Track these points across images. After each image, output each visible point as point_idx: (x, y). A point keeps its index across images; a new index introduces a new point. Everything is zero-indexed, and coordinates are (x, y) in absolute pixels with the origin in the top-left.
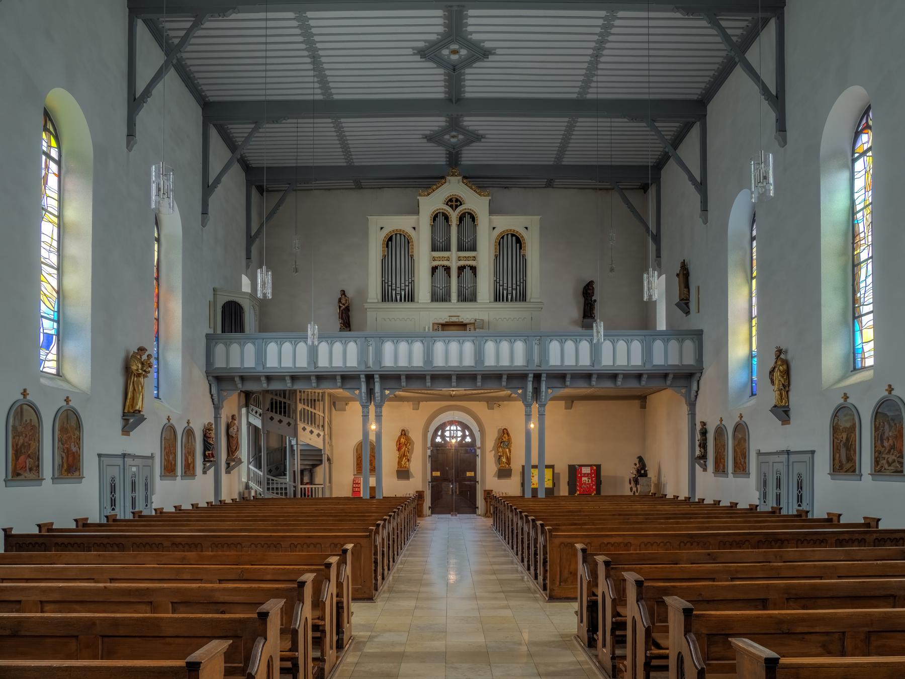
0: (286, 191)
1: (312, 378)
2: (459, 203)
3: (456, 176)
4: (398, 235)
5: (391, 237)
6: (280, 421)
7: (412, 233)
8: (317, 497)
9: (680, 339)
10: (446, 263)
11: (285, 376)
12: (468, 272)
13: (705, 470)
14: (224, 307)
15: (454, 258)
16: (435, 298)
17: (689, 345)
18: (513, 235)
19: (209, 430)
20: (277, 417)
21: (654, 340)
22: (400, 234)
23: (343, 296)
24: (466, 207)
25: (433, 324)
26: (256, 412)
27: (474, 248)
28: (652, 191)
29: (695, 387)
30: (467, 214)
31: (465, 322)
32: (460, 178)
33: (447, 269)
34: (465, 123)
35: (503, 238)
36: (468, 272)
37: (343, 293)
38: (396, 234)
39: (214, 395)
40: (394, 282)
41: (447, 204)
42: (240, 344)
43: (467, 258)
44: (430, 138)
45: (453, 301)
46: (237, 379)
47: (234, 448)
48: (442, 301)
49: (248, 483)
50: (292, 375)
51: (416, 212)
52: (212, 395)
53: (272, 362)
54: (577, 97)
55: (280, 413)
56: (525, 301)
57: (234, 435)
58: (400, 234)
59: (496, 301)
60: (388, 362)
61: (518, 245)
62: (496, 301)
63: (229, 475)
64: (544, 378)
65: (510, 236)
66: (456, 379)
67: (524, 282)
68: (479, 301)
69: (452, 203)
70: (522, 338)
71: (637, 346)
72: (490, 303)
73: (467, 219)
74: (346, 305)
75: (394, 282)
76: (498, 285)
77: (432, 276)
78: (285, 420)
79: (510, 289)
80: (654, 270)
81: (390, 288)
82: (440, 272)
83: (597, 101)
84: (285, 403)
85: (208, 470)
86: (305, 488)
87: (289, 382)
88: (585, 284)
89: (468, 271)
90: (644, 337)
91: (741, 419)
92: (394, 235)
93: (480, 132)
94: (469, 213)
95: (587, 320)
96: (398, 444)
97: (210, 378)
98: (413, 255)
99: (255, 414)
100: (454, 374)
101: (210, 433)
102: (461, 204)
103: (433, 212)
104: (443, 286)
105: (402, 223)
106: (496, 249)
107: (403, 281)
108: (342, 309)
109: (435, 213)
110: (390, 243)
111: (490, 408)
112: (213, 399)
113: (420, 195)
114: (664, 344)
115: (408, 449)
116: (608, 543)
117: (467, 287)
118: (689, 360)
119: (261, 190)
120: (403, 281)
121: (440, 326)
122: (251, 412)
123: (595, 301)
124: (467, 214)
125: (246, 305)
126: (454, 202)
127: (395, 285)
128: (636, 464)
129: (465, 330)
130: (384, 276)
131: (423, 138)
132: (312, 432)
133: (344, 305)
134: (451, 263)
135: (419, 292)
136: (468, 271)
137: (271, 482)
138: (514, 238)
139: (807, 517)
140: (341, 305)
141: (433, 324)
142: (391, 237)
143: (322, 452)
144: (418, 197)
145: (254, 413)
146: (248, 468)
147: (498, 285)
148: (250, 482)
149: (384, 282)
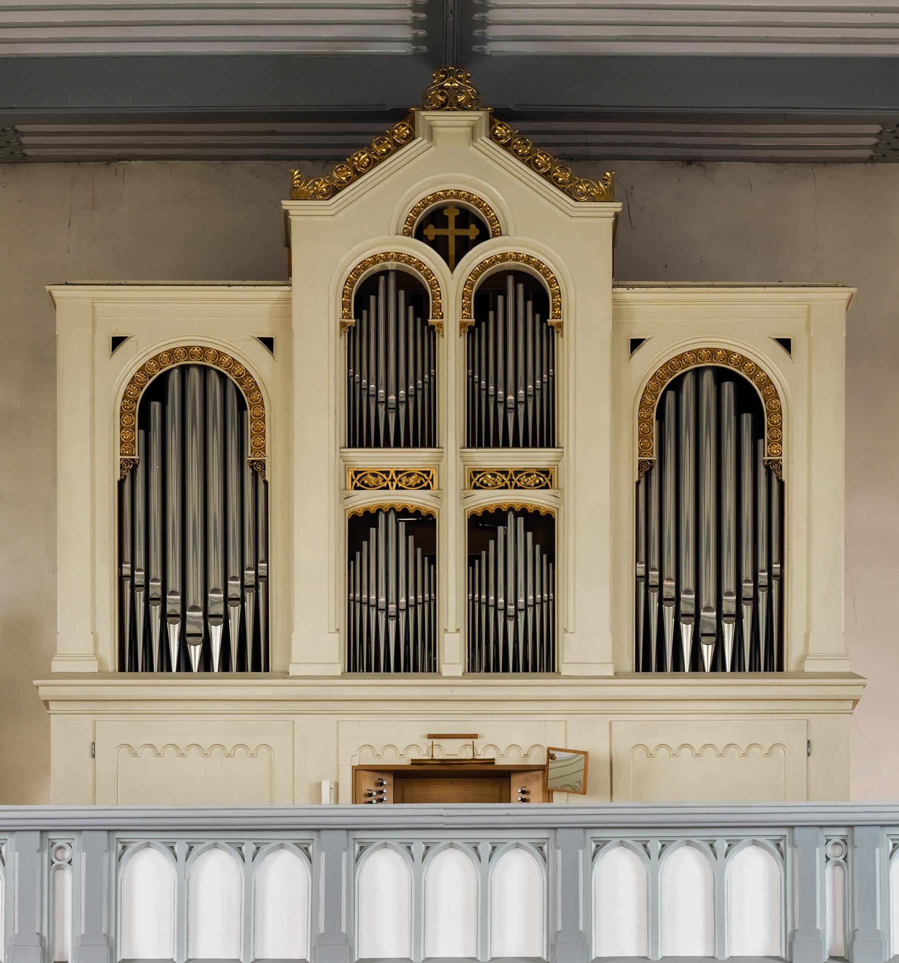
3: (461, 107)
5: (165, 377)
35: (676, 386)
61: (747, 418)
65: (708, 378)
98: (263, 463)
110: (156, 406)
138: (728, 388)
142: (164, 378)
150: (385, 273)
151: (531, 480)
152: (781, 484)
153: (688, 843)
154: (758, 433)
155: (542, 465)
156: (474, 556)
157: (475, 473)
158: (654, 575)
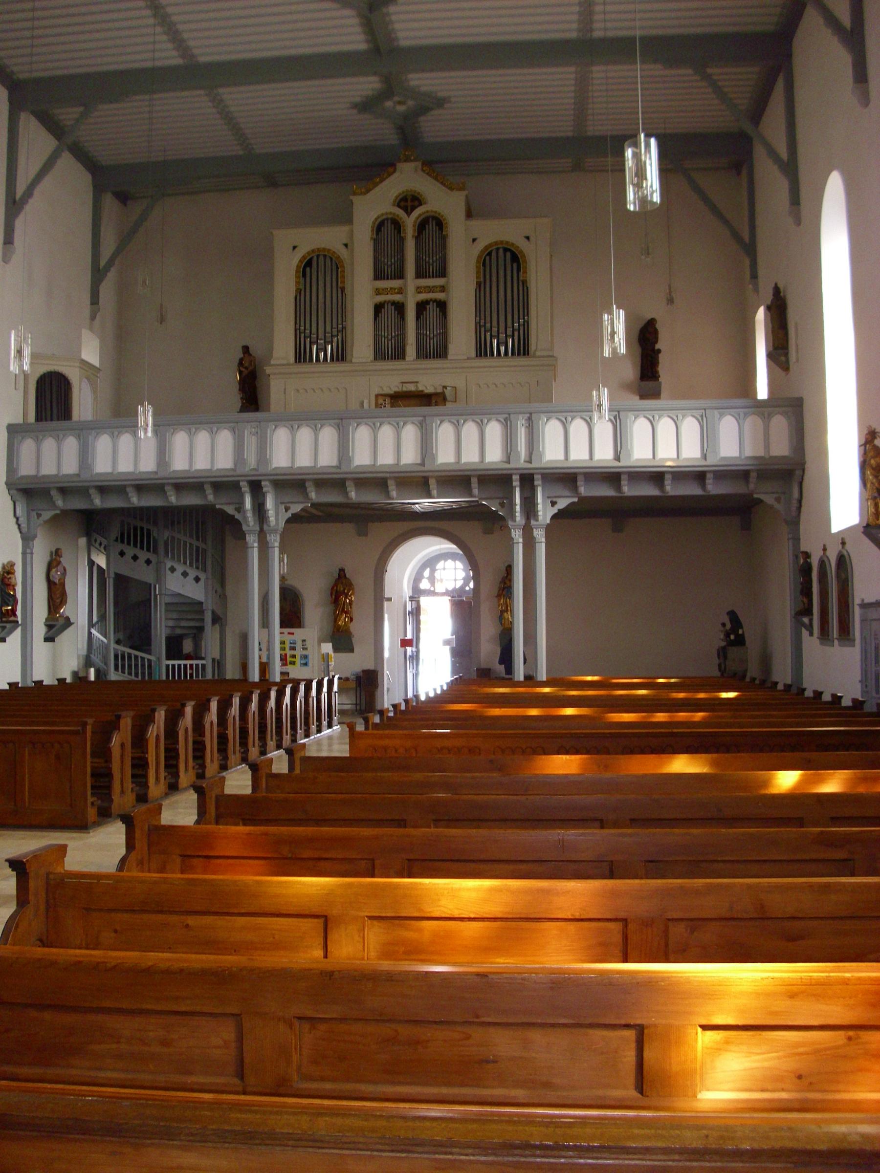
1: (166, 488)
2: (416, 203)
3: (411, 161)
4: (321, 259)
7: (343, 253)
9: (766, 414)
10: (397, 298)
11: (125, 486)
12: (432, 311)
13: (811, 634)
16: (380, 354)
17: (780, 424)
18: (506, 250)
19: (9, 573)
20: (130, 551)
21: (722, 416)
22: (325, 256)
23: (246, 355)
24: (429, 209)
25: (377, 396)
26: (100, 544)
27: (442, 272)
28: (744, 172)
29: (796, 495)
30: (431, 219)
31: (426, 391)
32: (419, 164)
33: (400, 308)
34: (412, 83)
35: (490, 254)
36: (432, 311)
38: (318, 256)
39: (20, 519)
40: (314, 330)
41: (399, 206)
42: (112, 436)
43: (431, 289)
44: (366, 106)
45: (407, 358)
46: (54, 493)
47: (58, 601)
48: (395, 359)
49: (90, 657)
50: (215, 482)
51: (345, 217)
52: (17, 519)
53: (102, 465)
55: (135, 545)
56: (528, 354)
57: (57, 581)
58: (325, 256)
59: (481, 355)
61: (515, 265)
62: (481, 355)
64: (538, 482)
66: (629, 480)
67: (526, 324)
68: (450, 357)
70: (332, 422)
71: (691, 427)
72: (468, 358)
73: (432, 226)
74: (250, 368)
75: (314, 330)
76: (483, 329)
77: (375, 319)
78: (143, 555)
79: (502, 336)
80: (618, 308)
82: (389, 313)
83: (603, 40)
84: (142, 529)
85: (8, 636)
86: (197, 665)
87: (209, 491)
88: (642, 324)
89: (432, 310)
90: (703, 411)
91: (843, 547)
92: (315, 257)
93: (440, 94)
94: (434, 218)
95: (651, 384)
97: (14, 492)
99: (98, 547)
100: (474, 476)
101: (10, 578)
102: (420, 204)
103: (376, 219)
104: (435, 333)
106: (478, 272)
107: (328, 329)
108: (244, 374)
109: (379, 220)
110: (308, 269)
112: (19, 526)
113: (355, 194)
114: (763, 421)
115: (351, 601)
116: (442, 749)
117: (432, 335)
118: (781, 448)
119: (123, 198)
120: (328, 329)
121: (388, 400)
122: (94, 543)
123: (659, 351)
124: (431, 219)
125: (73, 374)
126: (409, 201)
127: (315, 336)
128: (724, 625)
129: (429, 404)
130: (298, 322)
133: (246, 368)
134: (406, 297)
136: (432, 310)
137: (289, 659)
138: (508, 255)
139: (205, 677)
141: (377, 396)
143: (202, 607)
144: (351, 197)
145: (97, 545)
146: (90, 633)
147: (483, 329)
148: (92, 656)
149: (298, 331)
150: (387, 219)
155: (442, 284)
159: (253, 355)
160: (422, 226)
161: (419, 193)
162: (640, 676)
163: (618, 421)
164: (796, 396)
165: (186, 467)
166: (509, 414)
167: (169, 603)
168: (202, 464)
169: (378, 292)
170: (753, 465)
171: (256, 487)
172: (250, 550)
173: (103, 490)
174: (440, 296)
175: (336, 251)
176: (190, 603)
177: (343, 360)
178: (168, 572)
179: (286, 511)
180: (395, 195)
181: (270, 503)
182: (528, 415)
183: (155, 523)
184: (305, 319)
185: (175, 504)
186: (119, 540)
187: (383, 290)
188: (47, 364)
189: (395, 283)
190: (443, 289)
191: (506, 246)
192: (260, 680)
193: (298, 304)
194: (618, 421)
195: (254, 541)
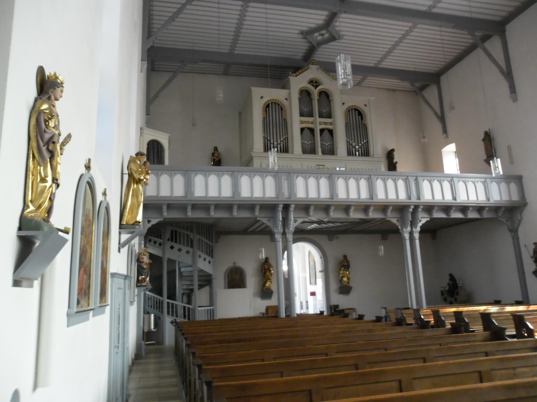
0: (174, 72)
3: (315, 65)
5: (269, 105)
6: (180, 250)
7: (286, 103)
8: (212, 319)
10: (311, 126)
14: (148, 144)
15: (319, 124)
16: (304, 152)
17: (513, 186)
18: (356, 110)
27: (329, 116)
33: (312, 130)
35: (349, 111)
37: (216, 149)
43: (326, 123)
51: (285, 86)
54: (427, 10)
60: (300, 194)
61: (360, 117)
63: (352, 290)
65: (353, 110)
69: (316, 84)
81: (269, 142)
88: (387, 152)
96: (263, 269)
98: (286, 119)
105: (278, 94)
108: (216, 161)
110: (267, 108)
111: (330, 239)
118: (515, 197)
123: (396, 162)
126: (315, 83)
131: (299, 34)
132: (205, 259)
135: (293, 146)
138: (357, 112)
140: (215, 158)
142: (269, 105)
150: (303, 90)
151: (329, 124)
152: (286, 122)
153: (246, 175)
154: (362, 119)
155: (331, 122)
156: (321, 135)
157: (301, 121)
158: (266, 136)
159: (219, 151)
160: (321, 93)
161: (318, 80)
162: (487, 302)
163: (453, 182)
164: (518, 174)
165: (249, 195)
166: (408, 176)
167: (200, 276)
168: (258, 194)
169: (302, 122)
170: (507, 204)
171: (286, 208)
172: (278, 243)
173: (195, 207)
174: (330, 127)
175: (282, 102)
176: (206, 276)
177: (288, 152)
178: (198, 258)
179: (295, 222)
180: (311, 77)
181: (292, 216)
182: (415, 177)
183: (192, 232)
184: (267, 131)
185: (236, 217)
186: (170, 239)
187: (304, 122)
188: (153, 135)
189: (310, 119)
190: (331, 124)
191: (356, 108)
192: (286, 316)
193: (266, 125)
194: (453, 182)
195: (280, 238)
